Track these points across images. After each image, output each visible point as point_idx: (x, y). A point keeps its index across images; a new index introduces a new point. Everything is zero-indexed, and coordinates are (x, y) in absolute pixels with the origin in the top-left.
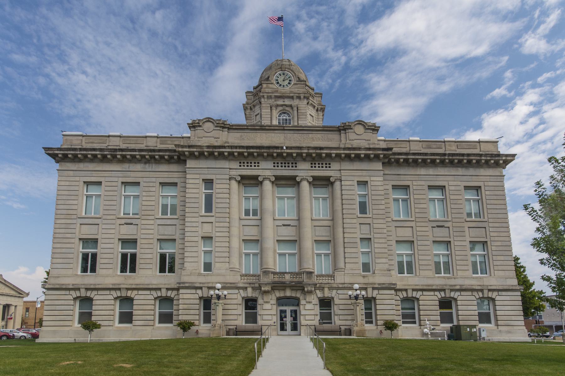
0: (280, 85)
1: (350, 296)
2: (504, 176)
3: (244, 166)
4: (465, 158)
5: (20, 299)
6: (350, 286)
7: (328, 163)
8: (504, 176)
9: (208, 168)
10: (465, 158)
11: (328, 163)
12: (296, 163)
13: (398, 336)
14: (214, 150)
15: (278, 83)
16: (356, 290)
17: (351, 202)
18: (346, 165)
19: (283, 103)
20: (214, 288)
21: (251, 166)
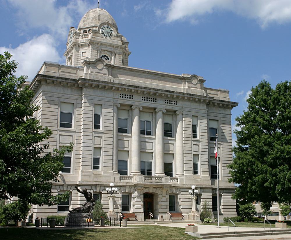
0: (105, 35)
1: (107, 191)
2: (231, 115)
3: (172, 103)
4: (181, 95)
5: (165, 197)
6: (189, 186)
7: (148, 97)
8: (231, 115)
9: (195, 109)
10: (181, 95)
11: (148, 97)
12: (132, 96)
13: (283, 224)
14: (180, 95)
15: (103, 33)
16: (112, 187)
17: (107, 118)
18: (187, 104)
19: (106, 49)
20: (108, 186)
21: (123, 97)
